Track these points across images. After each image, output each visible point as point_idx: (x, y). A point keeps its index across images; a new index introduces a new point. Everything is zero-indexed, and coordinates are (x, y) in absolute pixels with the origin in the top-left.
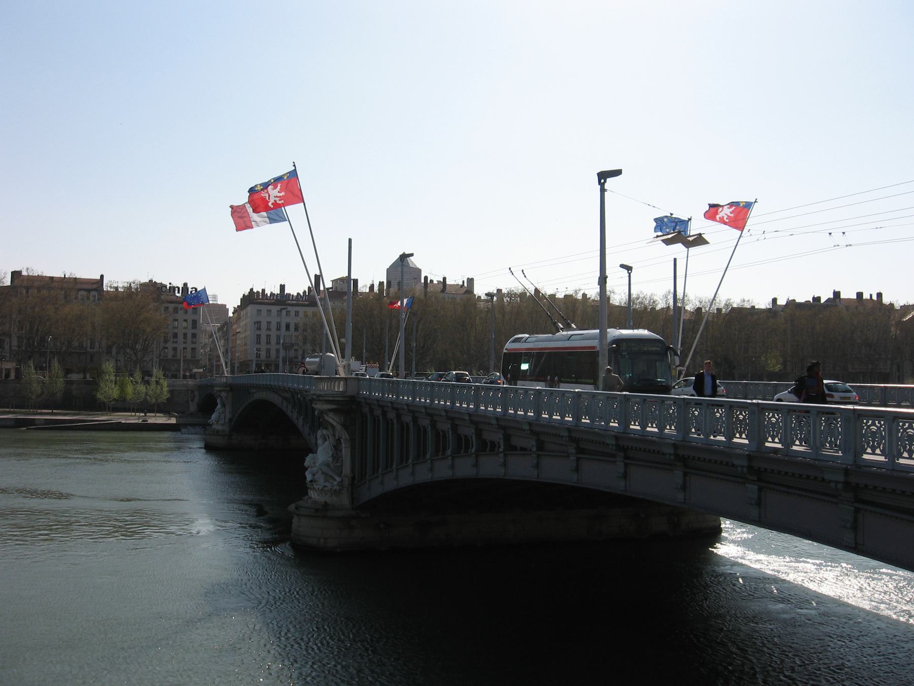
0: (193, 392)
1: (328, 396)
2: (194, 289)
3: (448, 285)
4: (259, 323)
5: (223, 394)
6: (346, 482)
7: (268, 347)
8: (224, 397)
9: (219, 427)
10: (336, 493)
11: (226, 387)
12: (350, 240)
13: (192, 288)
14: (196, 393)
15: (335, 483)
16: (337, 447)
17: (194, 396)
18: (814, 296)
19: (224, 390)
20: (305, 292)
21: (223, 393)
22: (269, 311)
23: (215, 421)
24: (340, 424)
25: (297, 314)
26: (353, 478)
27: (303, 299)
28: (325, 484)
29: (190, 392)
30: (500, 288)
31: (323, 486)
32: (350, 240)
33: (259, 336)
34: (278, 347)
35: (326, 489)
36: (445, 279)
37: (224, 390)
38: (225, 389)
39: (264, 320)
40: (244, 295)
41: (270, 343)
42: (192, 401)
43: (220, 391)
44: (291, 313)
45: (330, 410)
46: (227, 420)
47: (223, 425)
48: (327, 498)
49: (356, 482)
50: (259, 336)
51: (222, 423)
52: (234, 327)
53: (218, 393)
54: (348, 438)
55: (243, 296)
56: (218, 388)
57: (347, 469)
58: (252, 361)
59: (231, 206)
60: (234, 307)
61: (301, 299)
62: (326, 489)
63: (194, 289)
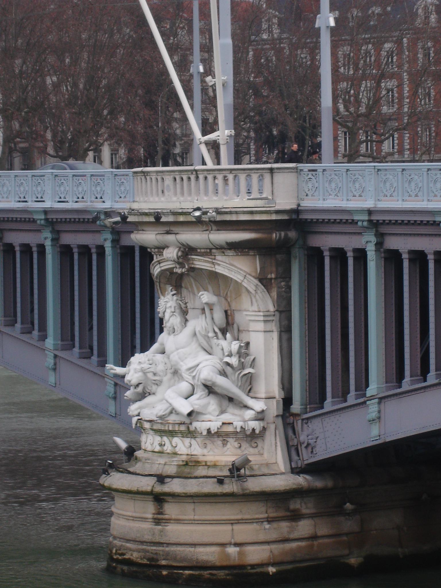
15: (249, 414)
26: (287, 401)
28: (226, 417)
49: (296, 407)
54: (272, 308)
62: (230, 429)
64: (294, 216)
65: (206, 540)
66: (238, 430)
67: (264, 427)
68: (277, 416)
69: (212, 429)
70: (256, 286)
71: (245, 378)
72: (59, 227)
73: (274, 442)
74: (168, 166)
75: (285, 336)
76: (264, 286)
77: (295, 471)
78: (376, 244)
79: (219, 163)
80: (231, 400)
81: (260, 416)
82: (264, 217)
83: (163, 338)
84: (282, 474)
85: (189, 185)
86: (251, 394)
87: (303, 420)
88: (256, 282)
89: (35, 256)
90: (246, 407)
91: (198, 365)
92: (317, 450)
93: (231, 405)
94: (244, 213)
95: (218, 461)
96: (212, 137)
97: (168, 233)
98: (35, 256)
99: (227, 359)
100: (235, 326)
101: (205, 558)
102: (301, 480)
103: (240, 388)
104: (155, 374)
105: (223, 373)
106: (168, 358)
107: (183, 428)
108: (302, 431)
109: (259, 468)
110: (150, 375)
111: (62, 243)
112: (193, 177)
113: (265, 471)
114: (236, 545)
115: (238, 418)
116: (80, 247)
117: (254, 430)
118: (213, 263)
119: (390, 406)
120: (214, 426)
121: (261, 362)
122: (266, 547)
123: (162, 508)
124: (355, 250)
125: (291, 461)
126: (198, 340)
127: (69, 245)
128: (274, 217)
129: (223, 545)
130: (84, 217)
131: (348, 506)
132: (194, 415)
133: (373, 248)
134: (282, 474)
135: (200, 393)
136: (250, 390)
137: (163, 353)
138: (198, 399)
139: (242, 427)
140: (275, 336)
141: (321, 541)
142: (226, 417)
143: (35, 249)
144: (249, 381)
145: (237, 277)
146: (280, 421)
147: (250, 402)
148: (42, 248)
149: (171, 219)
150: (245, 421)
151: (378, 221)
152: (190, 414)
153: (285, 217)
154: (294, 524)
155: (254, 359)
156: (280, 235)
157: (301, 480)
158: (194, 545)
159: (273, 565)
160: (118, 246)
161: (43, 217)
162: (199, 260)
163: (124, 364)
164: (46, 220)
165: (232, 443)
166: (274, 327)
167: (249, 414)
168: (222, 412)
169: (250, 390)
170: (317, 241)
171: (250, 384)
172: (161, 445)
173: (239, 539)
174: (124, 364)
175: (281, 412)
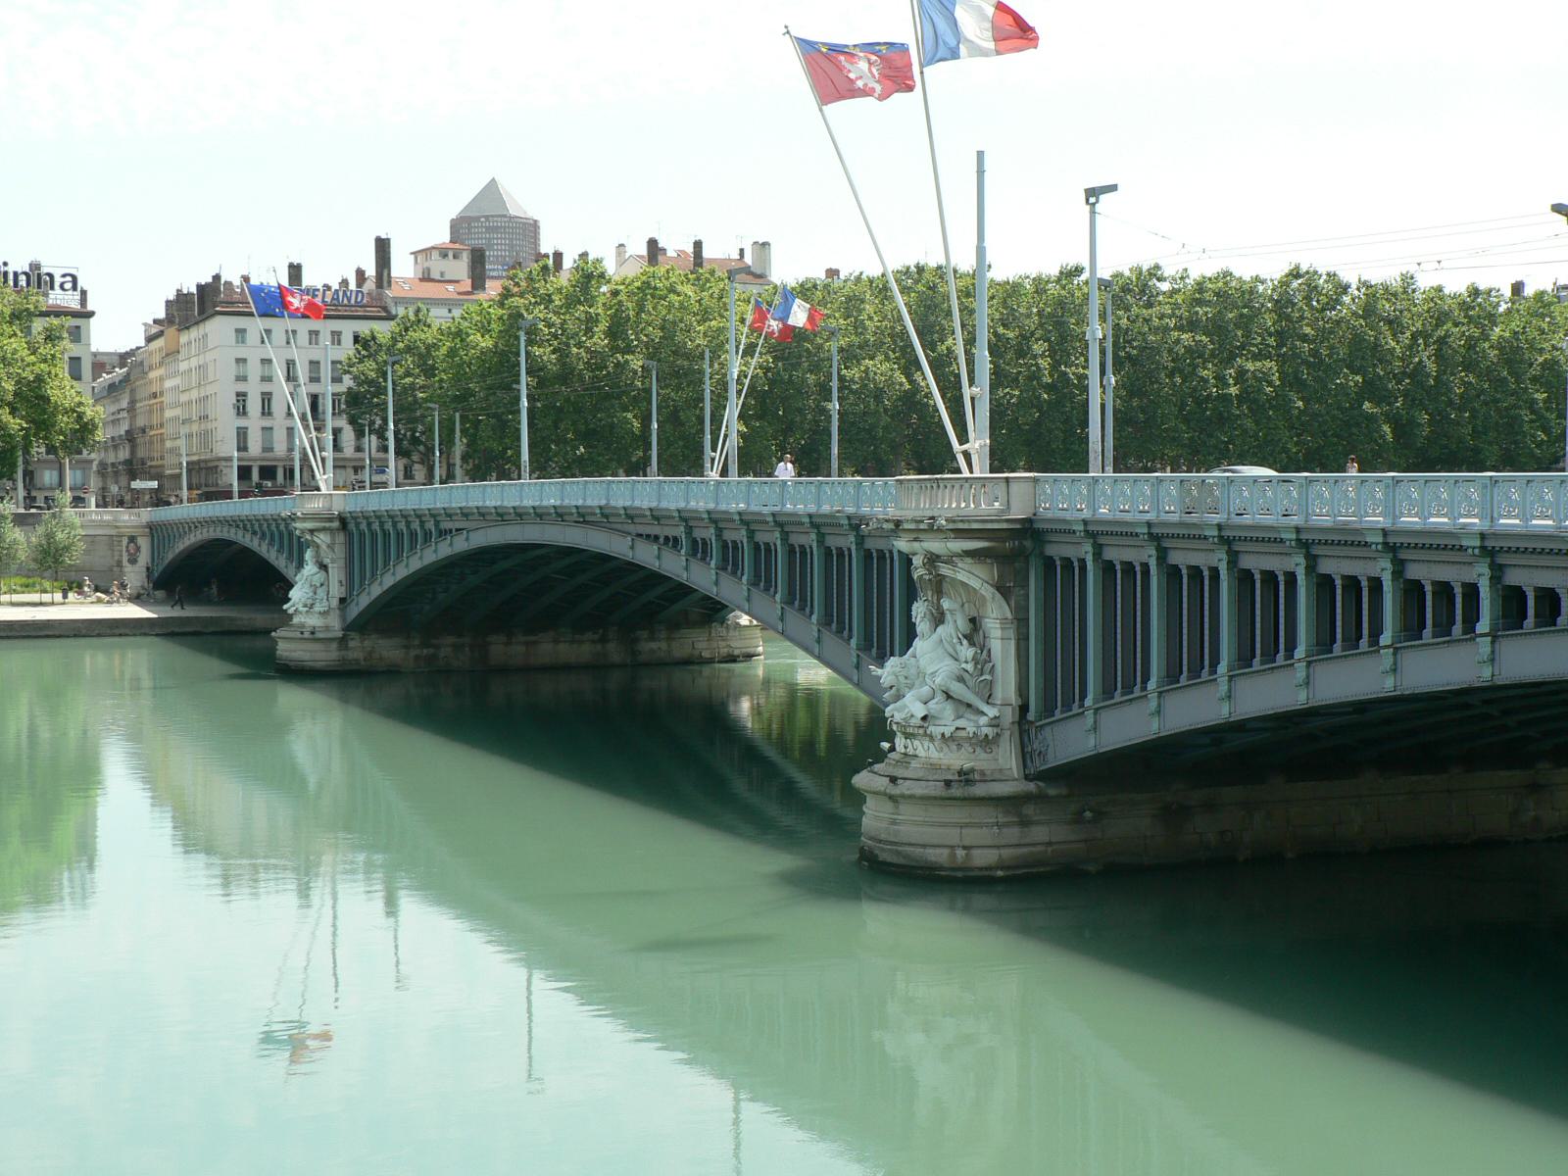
0: (132, 539)
1: (969, 521)
2: (69, 278)
3: (708, 259)
4: (241, 361)
5: (323, 539)
6: (1009, 716)
7: (267, 423)
8: (324, 547)
9: (313, 621)
10: (987, 743)
11: (330, 520)
12: (980, 155)
13: (64, 276)
14: (144, 543)
15: (983, 720)
16: (974, 631)
17: (138, 549)
18: (918, 264)
19: (324, 529)
20: (345, 283)
21: (322, 536)
22: (314, 334)
23: (305, 606)
24: (991, 585)
25: (336, 337)
26: (1024, 709)
27: (349, 300)
28: (961, 723)
29: (125, 541)
30: (834, 267)
31: (953, 729)
32: (980, 155)
33: (241, 397)
34: (288, 423)
35: (963, 734)
36: (698, 245)
37: (324, 529)
38: (327, 525)
39: (253, 353)
40: (1408, 279)
41: (270, 414)
42: (133, 561)
43: (312, 531)
44: (321, 335)
45: (968, 553)
46: (335, 603)
47: (324, 614)
48: (958, 759)
49: (1031, 716)
50: (241, 397)
51: (322, 610)
52: (153, 375)
53: (308, 537)
54: (1009, 615)
55: (178, 295)
56: (309, 525)
57: (1007, 687)
58: (229, 459)
59: (912, 91)
60: (145, 324)
61: (346, 302)
62: (963, 734)
63: (69, 278)
64: (1027, 525)
65: (935, 842)
66: (971, 735)
67: (997, 734)
68: (1013, 723)
69: (946, 733)
70: (993, 594)
71: (982, 685)
72: (1403, 555)
73: (1008, 748)
74: (1191, 472)
75: (1022, 643)
76: (1002, 594)
77: (1027, 778)
78: (1491, 578)
79: (971, 472)
80: (969, 705)
81: (994, 722)
82: (996, 526)
83: (917, 643)
84: (1017, 780)
85: (937, 493)
86: (990, 701)
87: (1037, 727)
88: (992, 590)
89: (1139, 577)
90: (983, 713)
91: (936, 672)
92: (1050, 756)
93: (968, 710)
94: (977, 521)
95: (951, 765)
96: (965, 447)
97: (916, 540)
98: (1139, 577)
99: (964, 665)
100: (981, 632)
101: (933, 859)
102: (1031, 787)
103: (977, 694)
104: (906, 678)
105: (961, 679)
106: (918, 661)
107: (921, 731)
108: (1036, 738)
109: (992, 773)
110: (902, 679)
111: (1507, 584)
112: (935, 485)
113: (997, 776)
114: (964, 848)
115: (972, 724)
116: (1263, 573)
117: (986, 735)
118: (954, 570)
119: (1104, 715)
120: (948, 731)
121: (999, 668)
122: (995, 852)
123: (897, 808)
124: (1465, 585)
125: (1025, 766)
126: (943, 646)
127: (1330, 575)
128: (1005, 526)
129: (952, 847)
130: (1163, 531)
131: (1088, 814)
132: (929, 719)
133: (1390, 577)
134: (1017, 780)
135: (940, 697)
136: (990, 695)
137: (915, 657)
138: (937, 703)
139: (974, 733)
140: (1013, 643)
141: (1055, 847)
142: (961, 723)
143: (1281, 578)
144: (988, 687)
145: (975, 583)
146: (1016, 726)
147: (985, 708)
148: (1291, 578)
149: (912, 526)
150: (979, 727)
151: (1493, 547)
152: (924, 718)
153: (1018, 526)
154: (1026, 829)
155: (993, 666)
156: (1014, 543)
157: (1031, 787)
158: (924, 846)
159: (1002, 869)
160: (1314, 574)
161: (1478, 543)
162: (944, 567)
163: (881, 666)
164: (1298, 540)
165: (967, 748)
166: (1011, 633)
167: (983, 720)
168: (959, 717)
169: (990, 695)
170: (1051, 550)
171: (990, 690)
172: (906, 748)
173: (967, 843)
174: (881, 666)
175: (1017, 719)
